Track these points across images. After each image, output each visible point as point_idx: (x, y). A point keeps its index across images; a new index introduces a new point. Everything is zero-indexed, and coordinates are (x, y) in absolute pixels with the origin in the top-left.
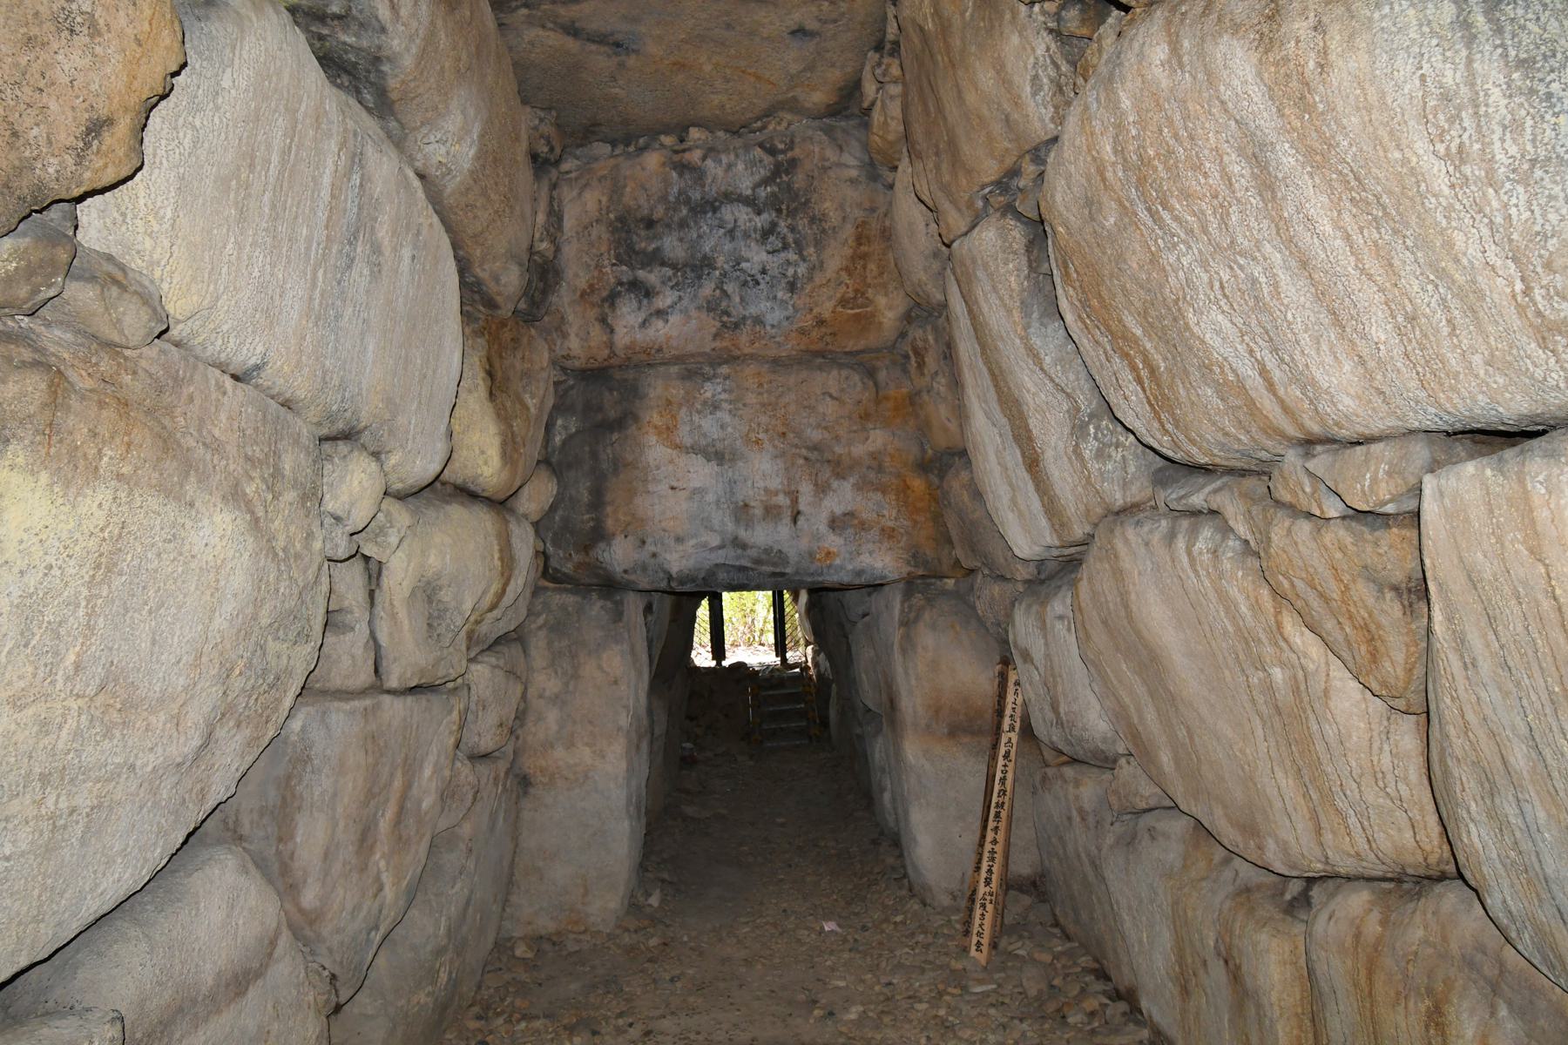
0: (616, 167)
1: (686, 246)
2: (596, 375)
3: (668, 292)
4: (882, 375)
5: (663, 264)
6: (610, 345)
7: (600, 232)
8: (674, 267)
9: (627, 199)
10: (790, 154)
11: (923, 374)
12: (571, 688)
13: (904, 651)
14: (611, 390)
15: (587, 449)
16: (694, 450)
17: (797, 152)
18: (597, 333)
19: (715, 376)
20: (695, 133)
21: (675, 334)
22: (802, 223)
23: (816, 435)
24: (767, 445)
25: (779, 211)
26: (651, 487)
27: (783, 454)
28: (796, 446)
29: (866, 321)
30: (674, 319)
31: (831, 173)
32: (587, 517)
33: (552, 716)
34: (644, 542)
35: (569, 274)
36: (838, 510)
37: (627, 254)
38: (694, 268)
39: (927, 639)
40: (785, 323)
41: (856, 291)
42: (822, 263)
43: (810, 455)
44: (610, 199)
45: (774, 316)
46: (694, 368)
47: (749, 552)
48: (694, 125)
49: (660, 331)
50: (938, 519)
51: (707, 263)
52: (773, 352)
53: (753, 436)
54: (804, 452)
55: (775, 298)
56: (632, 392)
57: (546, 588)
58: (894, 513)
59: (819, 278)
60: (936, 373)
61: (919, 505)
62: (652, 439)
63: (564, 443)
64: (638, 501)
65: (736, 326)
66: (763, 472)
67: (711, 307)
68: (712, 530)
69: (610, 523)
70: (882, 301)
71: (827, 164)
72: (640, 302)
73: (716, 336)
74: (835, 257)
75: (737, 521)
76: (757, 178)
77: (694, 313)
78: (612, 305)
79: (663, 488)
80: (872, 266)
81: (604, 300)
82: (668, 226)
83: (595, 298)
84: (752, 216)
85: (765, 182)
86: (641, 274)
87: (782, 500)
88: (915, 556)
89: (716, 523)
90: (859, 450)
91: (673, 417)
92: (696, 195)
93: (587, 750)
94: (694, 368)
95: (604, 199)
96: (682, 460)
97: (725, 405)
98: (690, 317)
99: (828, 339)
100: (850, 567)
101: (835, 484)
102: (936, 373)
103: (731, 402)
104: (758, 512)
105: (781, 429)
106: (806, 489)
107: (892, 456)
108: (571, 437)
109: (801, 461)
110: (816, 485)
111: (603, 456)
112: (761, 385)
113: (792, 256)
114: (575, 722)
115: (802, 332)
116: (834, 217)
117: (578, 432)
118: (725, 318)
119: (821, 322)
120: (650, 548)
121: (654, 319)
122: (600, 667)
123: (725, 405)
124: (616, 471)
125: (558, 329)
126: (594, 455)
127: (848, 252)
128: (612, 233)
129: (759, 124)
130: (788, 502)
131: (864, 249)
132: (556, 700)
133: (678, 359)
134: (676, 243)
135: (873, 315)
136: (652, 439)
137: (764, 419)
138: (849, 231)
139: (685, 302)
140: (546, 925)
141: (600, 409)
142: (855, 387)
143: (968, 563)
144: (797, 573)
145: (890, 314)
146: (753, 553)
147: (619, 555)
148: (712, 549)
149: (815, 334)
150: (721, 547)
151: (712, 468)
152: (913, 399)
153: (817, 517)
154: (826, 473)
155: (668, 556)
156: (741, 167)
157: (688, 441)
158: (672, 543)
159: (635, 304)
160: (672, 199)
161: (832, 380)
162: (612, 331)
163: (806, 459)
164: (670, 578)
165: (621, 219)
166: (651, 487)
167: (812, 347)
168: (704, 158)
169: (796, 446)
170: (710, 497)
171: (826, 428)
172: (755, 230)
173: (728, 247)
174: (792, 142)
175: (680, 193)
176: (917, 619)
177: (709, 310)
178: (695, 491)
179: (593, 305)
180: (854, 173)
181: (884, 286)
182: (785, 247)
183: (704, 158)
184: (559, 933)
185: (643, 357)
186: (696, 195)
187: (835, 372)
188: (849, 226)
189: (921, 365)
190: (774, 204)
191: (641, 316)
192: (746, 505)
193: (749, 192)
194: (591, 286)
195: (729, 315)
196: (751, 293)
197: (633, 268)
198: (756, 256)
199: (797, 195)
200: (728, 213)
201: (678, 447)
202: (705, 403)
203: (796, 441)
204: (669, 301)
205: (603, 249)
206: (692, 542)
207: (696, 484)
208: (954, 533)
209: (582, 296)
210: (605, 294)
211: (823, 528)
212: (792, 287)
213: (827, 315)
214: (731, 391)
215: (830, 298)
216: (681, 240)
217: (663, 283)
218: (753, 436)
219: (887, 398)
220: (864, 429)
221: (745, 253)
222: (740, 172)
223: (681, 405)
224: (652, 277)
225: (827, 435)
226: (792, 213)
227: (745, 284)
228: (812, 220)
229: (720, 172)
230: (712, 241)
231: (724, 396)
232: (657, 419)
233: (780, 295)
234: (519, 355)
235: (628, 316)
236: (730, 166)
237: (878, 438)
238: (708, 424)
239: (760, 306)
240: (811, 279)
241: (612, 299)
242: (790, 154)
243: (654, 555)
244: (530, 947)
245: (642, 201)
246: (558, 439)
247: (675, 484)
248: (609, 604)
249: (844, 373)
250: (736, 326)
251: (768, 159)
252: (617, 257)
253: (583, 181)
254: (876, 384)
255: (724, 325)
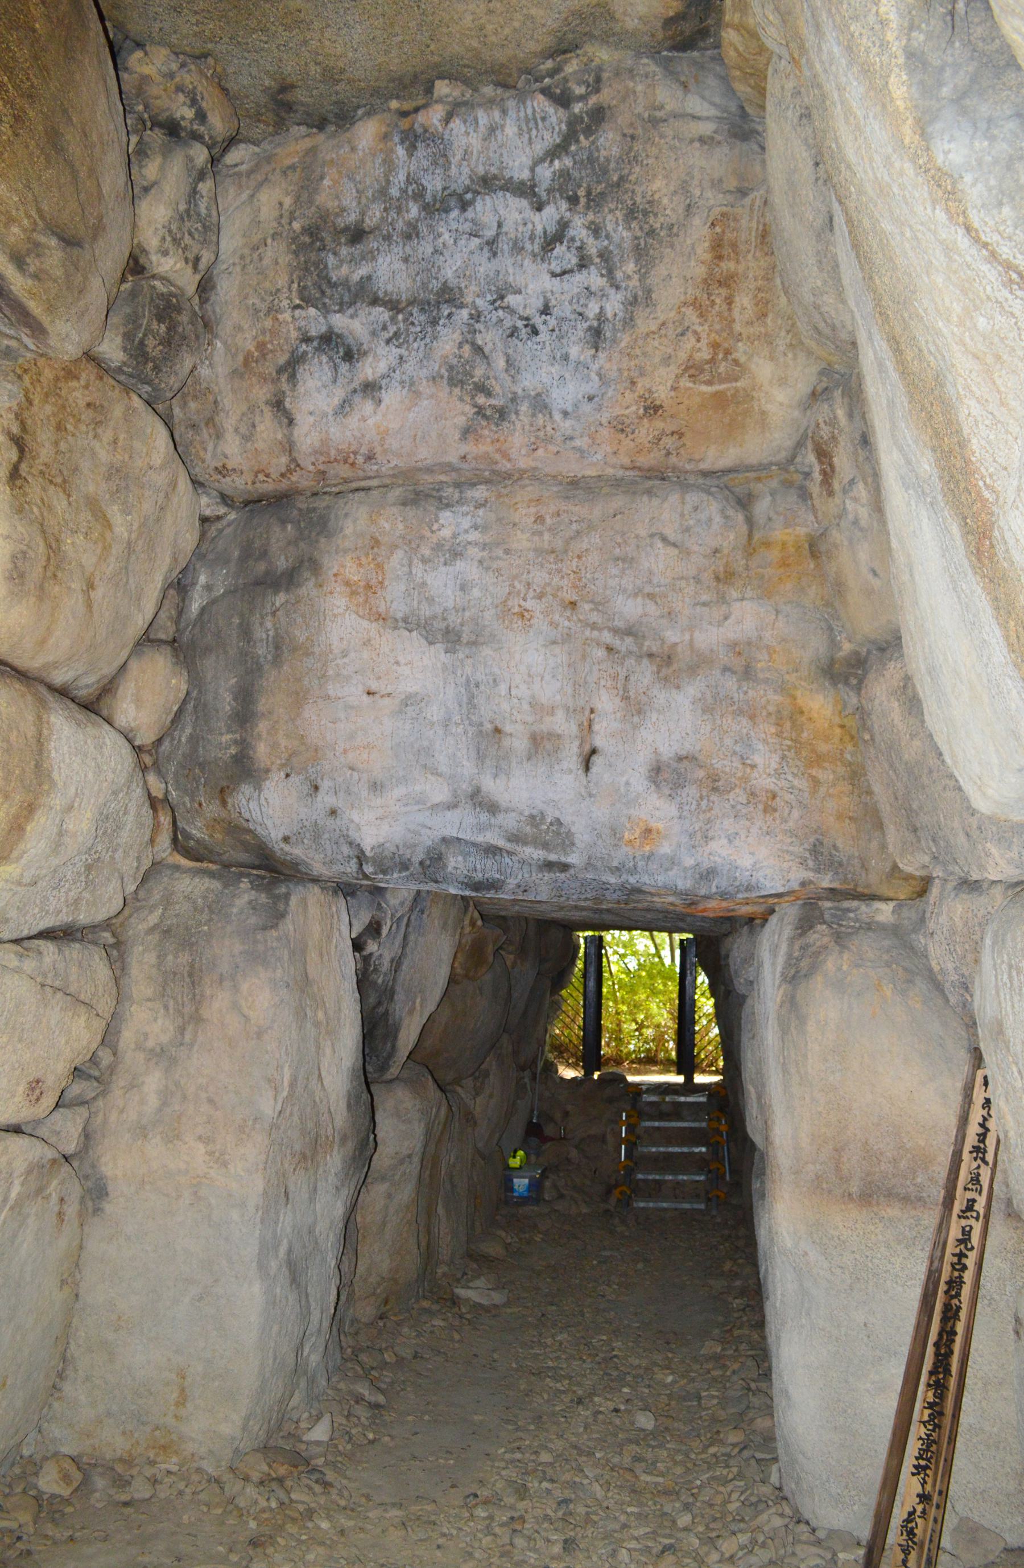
0: (312, 151)
1: (413, 268)
2: (268, 504)
3: (382, 349)
4: (762, 507)
5: (375, 301)
6: (289, 447)
7: (278, 255)
8: (394, 306)
9: (324, 199)
10: (593, 100)
11: (831, 493)
12: (188, 1037)
13: (784, 1030)
14: (283, 522)
15: (236, 621)
16: (408, 623)
17: (605, 96)
18: (268, 428)
19: (460, 502)
20: (442, 88)
21: (394, 425)
22: (613, 222)
23: (630, 608)
24: (539, 622)
25: (573, 200)
26: (332, 689)
27: (568, 637)
28: (594, 626)
29: (733, 408)
30: (392, 397)
31: (667, 130)
32: (226, 738)
33: (153, 1082)
34: (316, 788)
35: (225, 328)
36: (667, 751)
37: (317, 289)
38: (424, 306)
39: (825, 1008)
40: (587, 408)
41: (715, 346)
42: (649, 292)
43: (617, 643)
44: (297, 199)
45: (565, 394)
46: (422, 491)
47: (501, 819)
48: (441, 77)
49: (369, 421)
50: (856, 775)
51: (450, 295)
52: (572, 467)
53: (514, 603)
54: (607, 637)
55: (566, 358)
56: (318, 526)
57: (177, 868)
58: (774, 761)
59: (645, 323)
60: (852, 482)
61: (823, 747)
62: (338, 601)
63: (203, 610)
64: (309, 712)
65: (502, 414)
66: (529, 671)
67: (456, 377)
68: (436, 773)
69: (261, 751)
70: (763, 370)
71: (659, 114)
72: (336, 368)
73: (467, 432)
74: (677, 276)
75: (481, 757)
76: (539, 148)
77: (425, 387)
78: (293, 378)
79: (353, 692)
80: (744, 301)
81: (280, 371)
82: (388, 238)
83: (269, 368)
84: (529, 213)
85: (554, 153)
86: (339, 321)
87: (562, 724)
88: (820, 854)
89: (442, 761)
90: (710, 637)
91: (380, 566)
92: (434, 184)
93: (201, 1148)
94: (422, 491)
95: (288, 201)
96: (387, 641)
97: (473, 552)
98: (418, 394)
99: (669, 442)
100: (689, 862)
101: (661, 696)
102: (852, 482)
103: (484, 547)
104: (520, 744)
105: (571, 596)
106: (606, 702)
107: (770, 650)
108: (213, 602)
109: (600, 653)
110: (626, 698)
111: (259, 634)
112: (540, 519)
113: (594, 278)
114: (185, 1097)
115: (620, 427)
116: (671, 208)
117: (229, 592)
118: (481, 400)
119: (653, 409)
120: (326, 799)
121: (357, 399)
122: (235, 1006)
123: (473, 552)
124: (277, 660)
125: (210, 421)
126: (246, 632)
127: (701, 271)
128: (296, 253)
129: (549, 64)
130: (574, 729)
131: (728, 266)
132: (163, 1056)
133: (406, 475)
134: (399, 265)
135: (749, 397)
136: (338, 601)
137: (539, 577)
138: (698, 233)
139: (410, 367)
140: (113, 1442)
141: (264, 554)
142: (712, 524)
143: (912, 865)
144: (589, 865)
145: (781, 396)
146: (509, 821)
147: (273, 809)
148: (435, 807)
149: (645, 432)
150: (452, 806)
151: (435, 656)
152: (815, 548)
153: (626, 769)
154: (644, 674)
155: (355, 816)
156: (511, 130)
157: (400, 609)
158: (364, 793)
159: (328, 374)
160: (394, 192)
161: (667, 511)
162: (291, 422)
163: (610, 649)
164: (361, 858)
165: (312, 231)
166: (332, 689)
167: (643, 461)
168: (448, 119)
169: (594, 626)
170: (434, 712)
171: (651, 596)
172: (532, 238)
173: (485, 267)
174: (598, 80)
175: (408, 181)
176: (813, 969)
177: (452, 382)
178: (408, 701)
179: (264, 379)
180: (707, 128)
181: (768, 339)
182: (583, 264)
183: (448, 119)
184: (128, 1462)
185: (345, 471)
186: (434, 184)
187: (674, 498)
188: (697, 221)
189: (828, 475)
190: (565, 188)
191: (339, 394)
192: (497, 730)
193: (525, 175)
194: (261, 346)
195: (489, 394)
196: (524, 348)
197: (326, 310)
198: (534, 283)
199: (605, 171)
200: (488, 210)
201: (381, 618)
202: (438, 547)
203: (595, 617)
204: (382, 367)
205: (282, 281)
206: (399, 791)
207: (408, 687)
208: (885, 808)
209: (246, 363)
210: (282, 359)
211: (638, 782)
212: (596, 335)
213: (662, 394)
214: (485, 528)
215: (667, 360)
216: (406, 260)
217: (374, 334)
218: (514, 603)
219: (767, 544)
220: (722, 599)
221: (516, 277)
222: (515, 138)
223: (394, 547)
224: (355, 324)
225: (651, 608)
226: (595, 201)
227: (513, 332)
228: (631, 214)
229: (475, 141)
230: (455, 254)
231: (474, 536)
232: (352, 572)
233: (574, 351)
234: (107, 436)
235: (317, 391)
236: (492, 130)
237: (747, 617)
238: (442, 583)
239: (539, 372)
240: (629, 322)
241: (292, 367)
242: (593, 100)
243: (333, 812)
244: (66, 1478)
245: (349, 200)
246: (195, 607)
247: (374, 686)
248: (263, 898)
249: (693, 498)
250: (502, 414)
251: (556, 116)
252: (302, 290)
253: (260, 177)
254: (750, 521)
255: (480, 411)
